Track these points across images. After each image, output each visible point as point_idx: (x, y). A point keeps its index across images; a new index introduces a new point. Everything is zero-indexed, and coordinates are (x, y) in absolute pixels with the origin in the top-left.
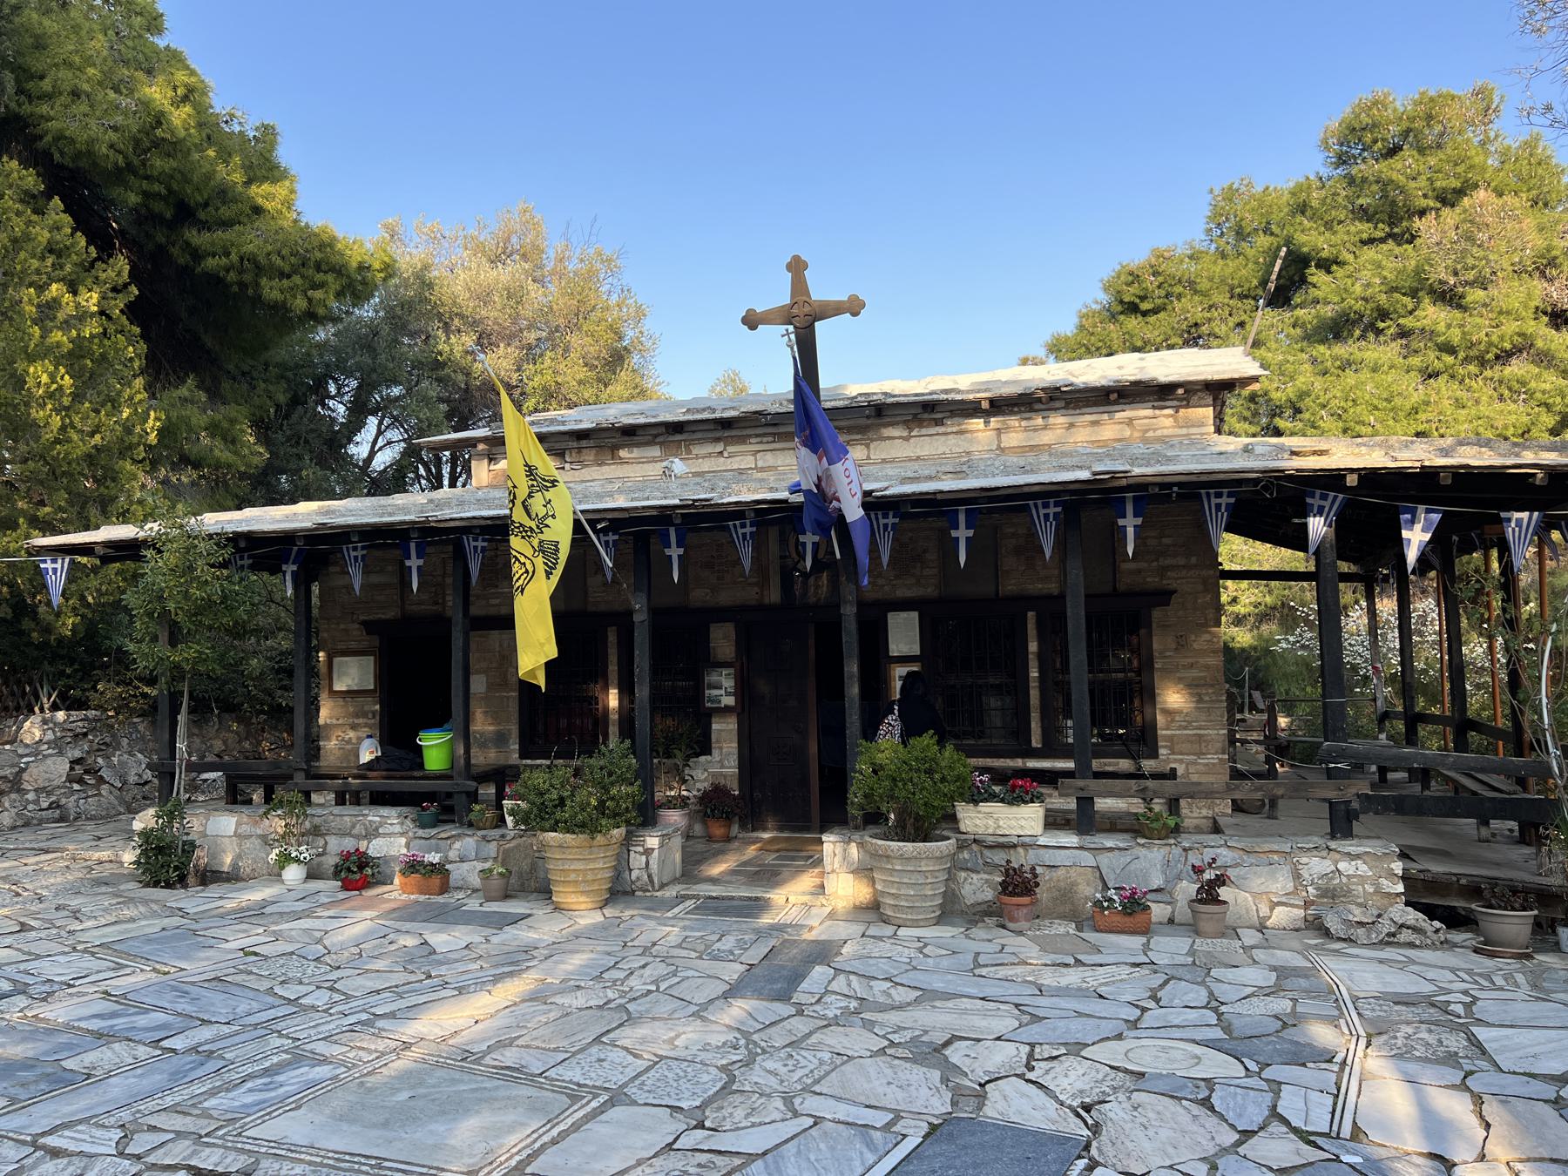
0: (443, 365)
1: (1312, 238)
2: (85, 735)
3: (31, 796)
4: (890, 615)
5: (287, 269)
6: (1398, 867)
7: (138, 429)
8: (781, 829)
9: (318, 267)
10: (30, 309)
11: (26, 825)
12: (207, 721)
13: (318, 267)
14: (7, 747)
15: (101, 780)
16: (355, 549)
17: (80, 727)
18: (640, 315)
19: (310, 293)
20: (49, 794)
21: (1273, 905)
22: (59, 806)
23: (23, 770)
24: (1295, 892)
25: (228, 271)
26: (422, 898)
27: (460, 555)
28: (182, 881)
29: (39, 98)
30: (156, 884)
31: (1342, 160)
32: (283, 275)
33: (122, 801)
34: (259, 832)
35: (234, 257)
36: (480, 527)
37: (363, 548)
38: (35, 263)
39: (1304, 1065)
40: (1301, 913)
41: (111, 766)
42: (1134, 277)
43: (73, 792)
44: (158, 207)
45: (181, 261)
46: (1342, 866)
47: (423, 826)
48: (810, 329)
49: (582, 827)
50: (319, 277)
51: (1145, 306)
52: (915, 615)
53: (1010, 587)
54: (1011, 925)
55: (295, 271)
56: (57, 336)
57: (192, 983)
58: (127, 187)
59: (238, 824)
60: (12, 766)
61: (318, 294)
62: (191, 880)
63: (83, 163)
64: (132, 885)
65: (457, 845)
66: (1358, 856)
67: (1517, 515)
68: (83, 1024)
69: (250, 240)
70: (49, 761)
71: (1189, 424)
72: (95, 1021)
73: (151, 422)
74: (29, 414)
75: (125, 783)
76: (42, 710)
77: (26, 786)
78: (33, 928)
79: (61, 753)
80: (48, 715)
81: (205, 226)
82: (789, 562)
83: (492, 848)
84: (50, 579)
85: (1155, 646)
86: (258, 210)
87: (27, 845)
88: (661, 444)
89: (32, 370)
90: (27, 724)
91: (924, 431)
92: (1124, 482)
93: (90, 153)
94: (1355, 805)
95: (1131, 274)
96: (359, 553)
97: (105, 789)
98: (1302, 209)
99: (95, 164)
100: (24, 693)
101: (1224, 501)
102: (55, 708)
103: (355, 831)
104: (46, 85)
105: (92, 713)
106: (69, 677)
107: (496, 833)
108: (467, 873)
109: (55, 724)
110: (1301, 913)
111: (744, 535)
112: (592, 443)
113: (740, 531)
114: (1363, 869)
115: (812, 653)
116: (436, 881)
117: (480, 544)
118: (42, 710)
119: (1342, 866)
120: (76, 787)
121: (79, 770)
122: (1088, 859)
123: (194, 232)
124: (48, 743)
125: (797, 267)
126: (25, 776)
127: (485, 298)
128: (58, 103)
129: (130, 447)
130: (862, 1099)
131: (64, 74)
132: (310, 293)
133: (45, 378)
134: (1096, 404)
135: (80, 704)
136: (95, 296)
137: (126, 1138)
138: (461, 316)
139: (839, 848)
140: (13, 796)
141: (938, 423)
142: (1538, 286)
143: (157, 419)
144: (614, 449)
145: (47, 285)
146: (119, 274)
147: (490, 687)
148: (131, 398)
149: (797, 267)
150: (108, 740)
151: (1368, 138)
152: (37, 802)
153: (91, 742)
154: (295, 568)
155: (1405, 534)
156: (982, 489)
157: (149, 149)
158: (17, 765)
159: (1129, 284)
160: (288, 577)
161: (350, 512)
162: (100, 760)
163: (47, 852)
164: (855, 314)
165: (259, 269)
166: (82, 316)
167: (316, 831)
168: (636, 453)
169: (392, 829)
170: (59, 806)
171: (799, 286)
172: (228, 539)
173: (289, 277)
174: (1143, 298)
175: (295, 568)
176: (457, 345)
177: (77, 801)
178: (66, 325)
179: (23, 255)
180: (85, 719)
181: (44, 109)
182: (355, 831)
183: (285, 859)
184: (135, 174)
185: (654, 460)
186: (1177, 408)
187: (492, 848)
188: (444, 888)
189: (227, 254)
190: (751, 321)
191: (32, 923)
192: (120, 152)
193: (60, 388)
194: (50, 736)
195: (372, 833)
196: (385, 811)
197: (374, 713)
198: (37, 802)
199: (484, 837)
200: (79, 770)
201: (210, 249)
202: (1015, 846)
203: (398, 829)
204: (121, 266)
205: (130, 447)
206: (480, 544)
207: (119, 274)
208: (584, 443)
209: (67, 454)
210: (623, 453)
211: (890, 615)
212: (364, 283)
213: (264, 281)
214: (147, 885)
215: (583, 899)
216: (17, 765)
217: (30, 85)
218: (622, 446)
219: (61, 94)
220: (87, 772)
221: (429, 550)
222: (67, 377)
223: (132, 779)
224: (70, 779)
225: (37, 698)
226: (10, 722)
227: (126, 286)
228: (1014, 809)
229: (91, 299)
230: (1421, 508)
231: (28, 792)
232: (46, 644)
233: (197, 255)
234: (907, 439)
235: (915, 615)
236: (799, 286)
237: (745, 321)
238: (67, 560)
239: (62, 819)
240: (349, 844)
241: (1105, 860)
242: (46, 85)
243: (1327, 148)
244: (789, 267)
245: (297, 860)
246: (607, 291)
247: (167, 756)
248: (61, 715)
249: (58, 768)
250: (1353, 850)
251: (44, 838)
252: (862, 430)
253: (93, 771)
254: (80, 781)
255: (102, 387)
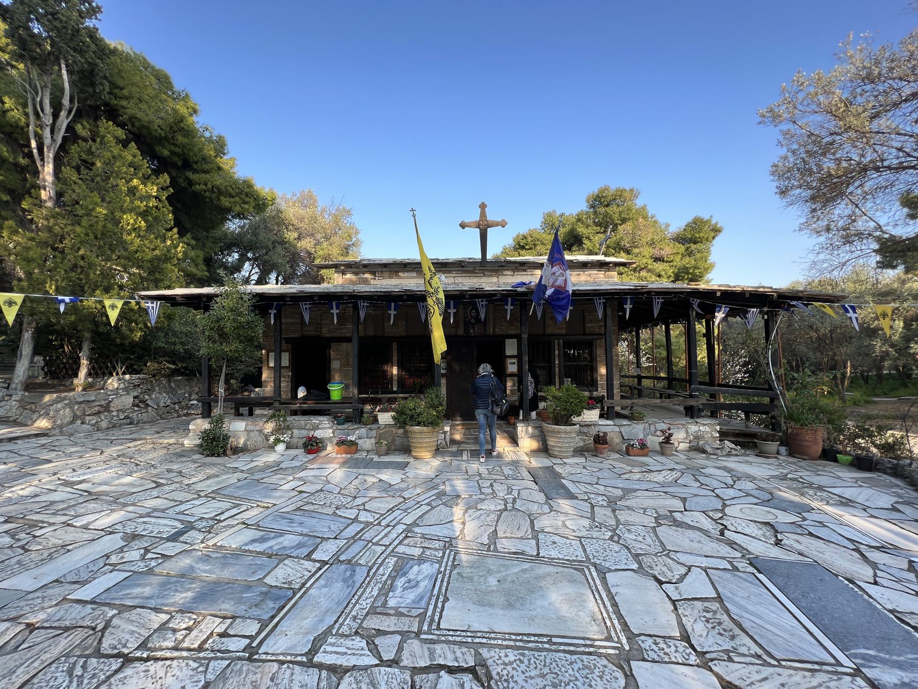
0: (286, 243)
1: (581, 230)
2: (139, 385)
3: (115, 413)
4: (506, 340)
5: (234, 194)
6: (718, 428)
7: (173, 251)
8: (463, 420)
9: (247, 195)
10: (125, 189)
11: (114, 426)
12: (192, 379)
13: (247, 195)
14: (102, 391)
15: (148, 405)
16: (306, 304)
17: (137, 382)
18: (357, 233)
19: (242, 205)
20: (123, 412)
21: (679, 443)
22: (128, 418)
23: (111, 402)
24: (686, 438)
25: (205, 192)
26: (349, 456)
27: (356, 308)
28: (225, 454)
29: (121, 98)
30: (213, 455)
31: (592, 206)
32: (231, 196)
33: (158, 414)
34: (257, 428)
35: (209, 186)
36: (378, 296)
37: (309, 304)
38: (124, 169)
39: (809, 512)
40: (688, 445)
41: (152, 399)
42: (525, 237)
43: (135, 411)
44: (176, 159)
45: (183, 185)
46: (701, 428)
47: (338, 424)
48: (486, 231)
49: (432, 423)
50: (247, 199)
51: (527, 247)
52: (516, 340)
53: (549, 331)
54: (601, 456)
55: (238, 194)
56: (138, 203)
57: (288, 513)
58: (164, 147)
59: (246, 425)
60: (105, 400)
61: (246, 206)
62: (228, 452)
63: (144, 132)
64: (198, 456)
65: (357, 432)
66: (706, 425)
67: (753, 310)
68: (251, 548)
69: (218, 180)
70: (123, 398)
71: (609, 277)
72: (257, 544)
73: (179, 249)
74: (122, 238)
75: (159, 406)
76: (117, 374)
77: (111, 409)
78: (163, 485)
79: (128, 394)
80: (121, 376)
81: (195, 171)
82: (467, 319)
83: (374, 433)
84: (150, 311)
85: (598, 353)
86: (220, 168)
87: (122, 437)
88: (417, 271)
89: (125, 216)
90: (109, 381)
91: (519, 273)
92: (645, 290)
93: (148, 128)
94: (701, 407)
95: (524, 236)
96: (308, 306)
97: (150, 409)
98: (579, 220)
99: (150, 133)
100: (107, 367)
101: (660, 300)
102: (124, 373)
103: (308, 427)
104: (125, 92)
105: (142, 376)
106: (131, 359)
107: (374, 426)
108: (367, 443)
109: (125, 381)
110: (688, 445)
111: (482, 305)
112: (387, 269)
113: (481, 303)
114: (708, 429)
115: (475, 354)
116: (354, 448)
117: (366, 304)
118: (117, 374)
119: (701, 428)
120: (136, 408)
121: (137, 401)
122: (617, 429)
123: (191, 173)
124: (122, 389)
125: (483, 206)
126: (112, 404)
127: (302, 219)
128: (131, 102)
129: (171, 258)
130: (704, 554)
131: (134, 89)
132: (242, 205)
133: (132, 221)
134: (579, 268)
135: (138, 373)
136: (155, 188)
137: (145, 554)
138: (293, 225)
139: (524, 429)
140: (106, 414)
141: (525, 270)
142: (651, 250)
143: (182, 247)
144: (397, 272)
145: (131, 180)
146: (165, 181)
147: (341, 366)
148: (171, 237)
149: (483, 206)
150: (149, 388)
151: (603, 200)
152: (118, 416)
153: (142, 388)
154: (275, 311)
155: (716, 314)
156: (594, 290)
157: (176, 132)
158: (108, 399)
159: (523, 239)
160: (272, 316)
161: (310, 288)
162: (146, 397)
163: (135, 440)
164: (503, 227)
165: (220, 192)
166: (149, 197)
167: (288, 428)
168: (406, 274)
169: (325, 426)
170: (128, 418)
171: (483, 214)
172: (253, 296)
173: (233, 197)
174: (526, 244)
175: (275, 311)
176: (291, 236)
177: (137, 415)
178: (141, 199)
179: (118, 164)
180: (139, 378)
181: (124, 103)
182: (308, 427)
183: (277, 441)
184: (168, 142)
185: (414, 278)
186: (605, 272)
187: (374, 433)
188: (357, 451)
189: (206, 185)
190: (463, 226)
191: (161, 481)
192: (163, 130)
193: (140, 227)
194: (122, 386)
195: (316, 428)
196: (321, 418)
197: (288, 376)
198: (118, 416)
199: (370, 429)
200: (137, 401)
201: (198, 181)
202: (591, 425)
203: (328, 426)
204: (165, 179)
205: (171, 258)
206: (366, 304)
207: (165, 181)
208: (384, 269)
209: (142, 258)
210: (400, 274)
211: (506, 340)
212: (263, 204)
213: (222, 198)
214: (208, 456)
215: (428, 454)
216: (108, 399)
217: (116, 91)
218: (401, 272)
219: (133, 98)
220: (140, 402)
221: (341, 306)
222: (143, 222)
223: (162, 404)
224: (133, 405)
225: (114, 368)
226: (99, 380)
227: (167, 187)
228: (590, 412)
229: (153, 190)
230: (724, 306)
231: (113, 411)
232: (122, 344)
233: (191, 183)
234: (513, 276)
235: (516, 340)
236: (483, 214)
237: (460, 225)
238: (159, 303)
239: (131, 423)
240: (304, 433)
241: (623, 429)
242: (125, 92)
243: (588, 202)
244: (480, 206)
245: (284, 441)
246: (346, 222)
247: (207, 395)
248: (127, 377)
249: (128, 400)
250: (705, 422)
251: (128, 433)
252: (496, 271)
253: (144, 402)
254: (137, 406)
255: (155, 230)
